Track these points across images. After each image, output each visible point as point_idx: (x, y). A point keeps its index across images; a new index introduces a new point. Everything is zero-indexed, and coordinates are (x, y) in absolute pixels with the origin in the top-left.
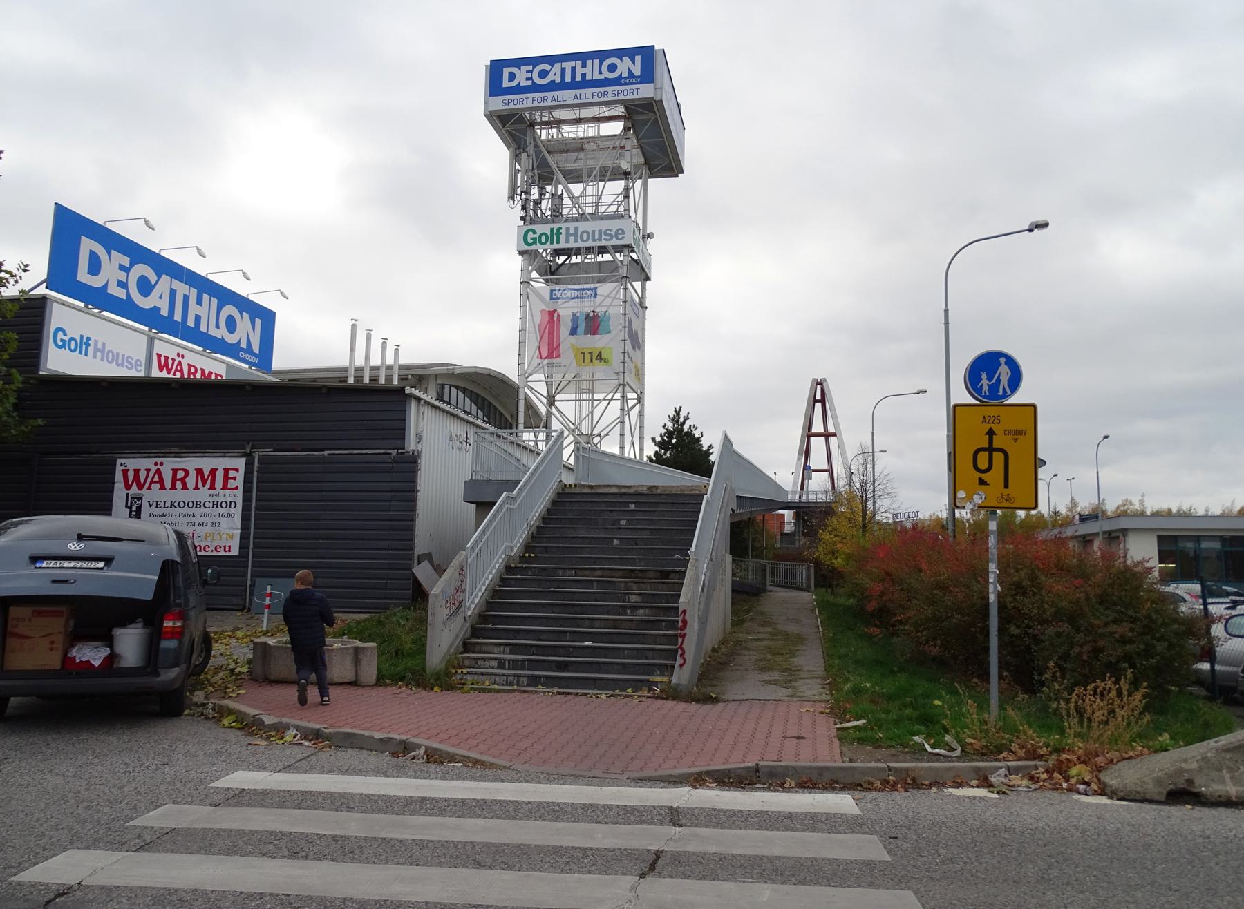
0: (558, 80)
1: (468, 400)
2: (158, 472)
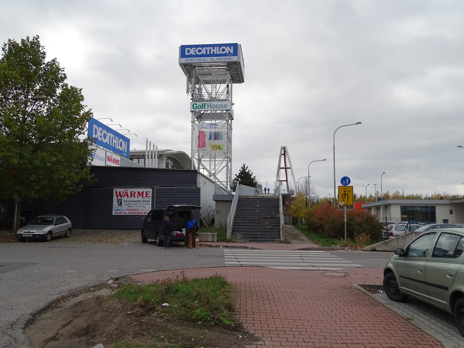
0: (205, 53)
1: (171, 162)
2: (126, 192)
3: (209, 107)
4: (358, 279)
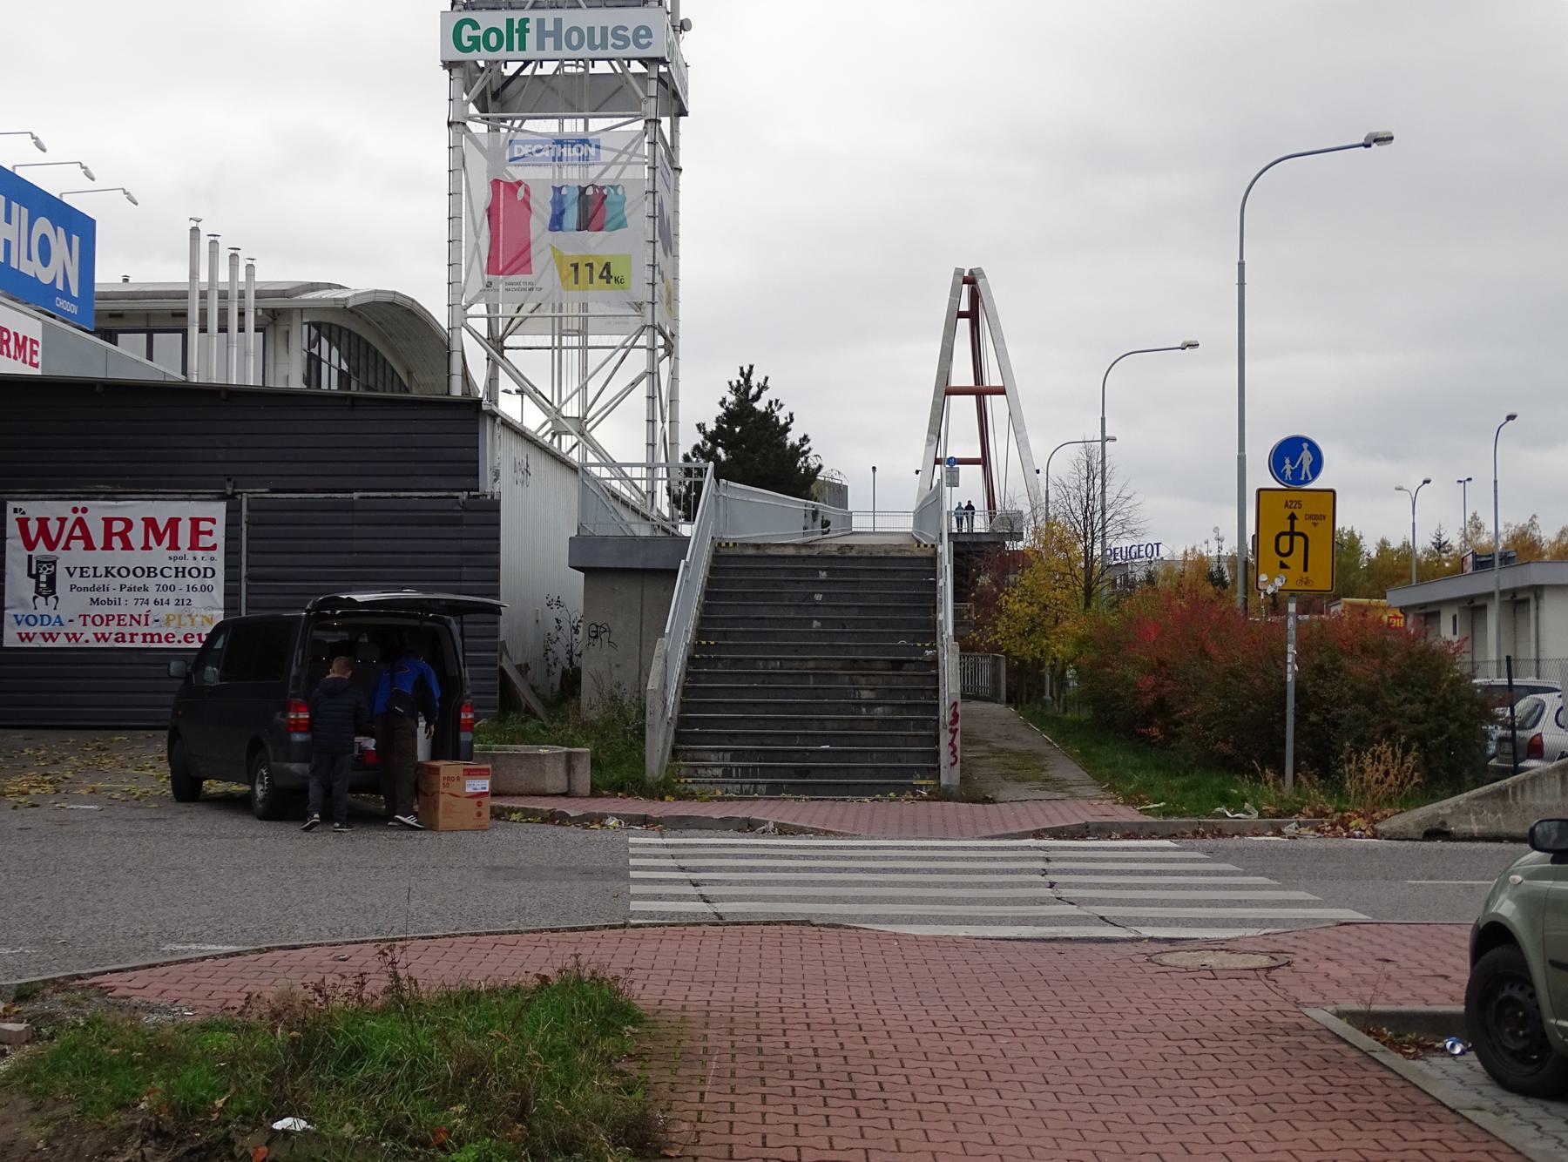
1: (335, 351)
2: (80, 522)
3: (549, 42)
4: (1339, 984)
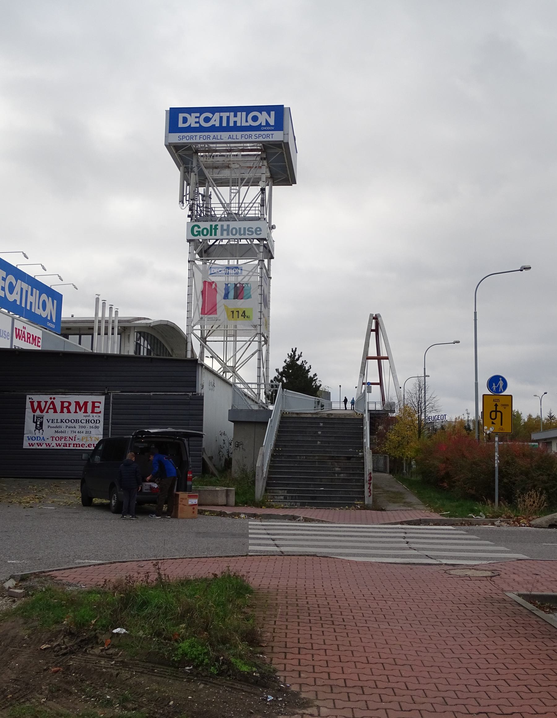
0: (217, 125)
1: (146, 342)
2: (52, 403)
3: (225, 233)
